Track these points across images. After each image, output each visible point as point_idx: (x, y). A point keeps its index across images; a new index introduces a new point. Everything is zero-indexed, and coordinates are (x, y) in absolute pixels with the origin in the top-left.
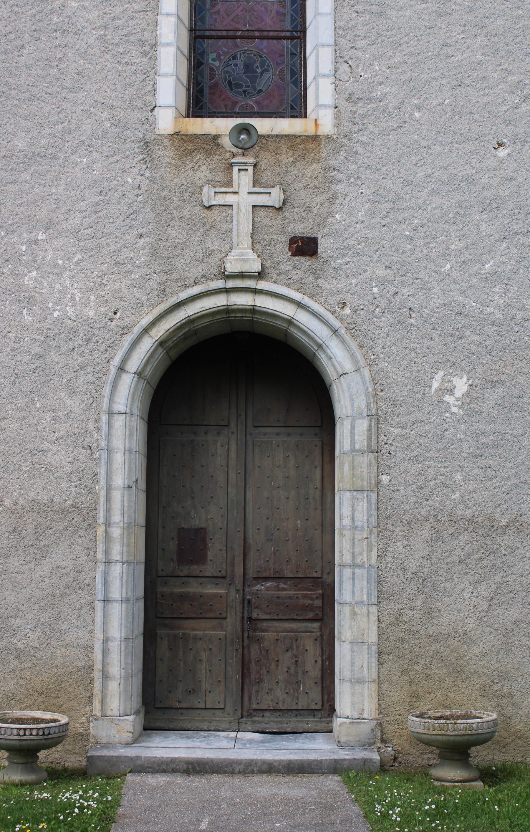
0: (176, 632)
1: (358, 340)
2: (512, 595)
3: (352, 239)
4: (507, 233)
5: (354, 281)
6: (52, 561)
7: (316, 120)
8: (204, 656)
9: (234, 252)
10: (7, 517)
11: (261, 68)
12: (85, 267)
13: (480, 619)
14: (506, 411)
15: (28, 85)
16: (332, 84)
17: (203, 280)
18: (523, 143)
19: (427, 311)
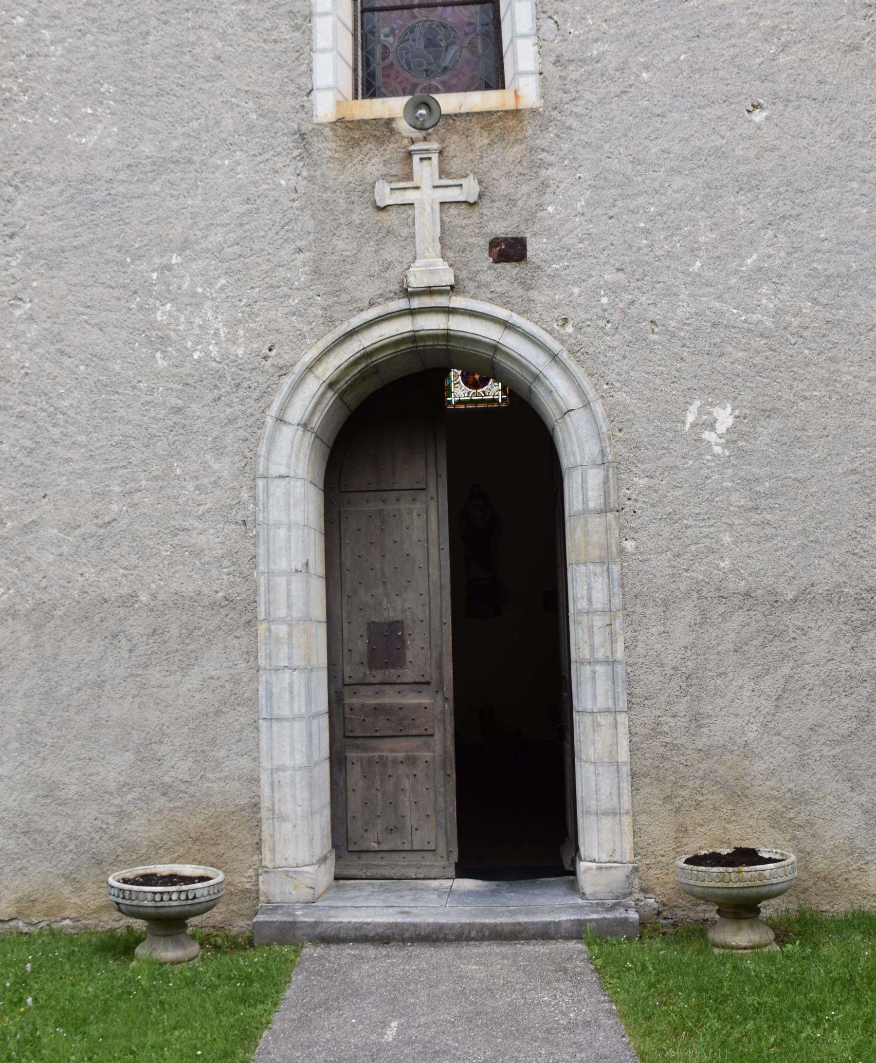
0: (371, 754)
1: (585, 366)
2: (806, 692)
3: (570, 236)
4: (772, 218)
5: (576, 290)
6: (203, 670)
7: (516, 91)
8: (407, 784)
9: (419, 262)
10: (145, 616)
11: (446, 40)
12: (231, 294)
13: (765, 725)
14: (785, 448)
15: (156, 78)
16: (534, 45)
17: (380, 300)
18: (785, 103)
19: (673, 324)
